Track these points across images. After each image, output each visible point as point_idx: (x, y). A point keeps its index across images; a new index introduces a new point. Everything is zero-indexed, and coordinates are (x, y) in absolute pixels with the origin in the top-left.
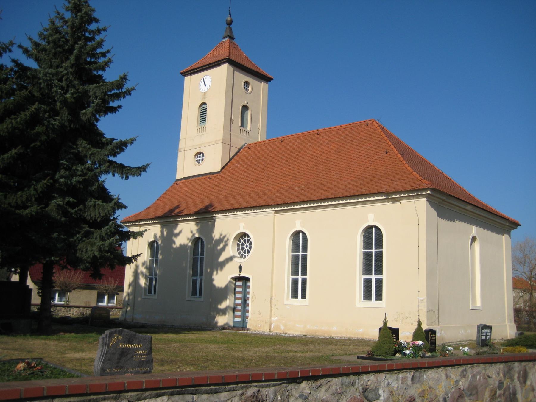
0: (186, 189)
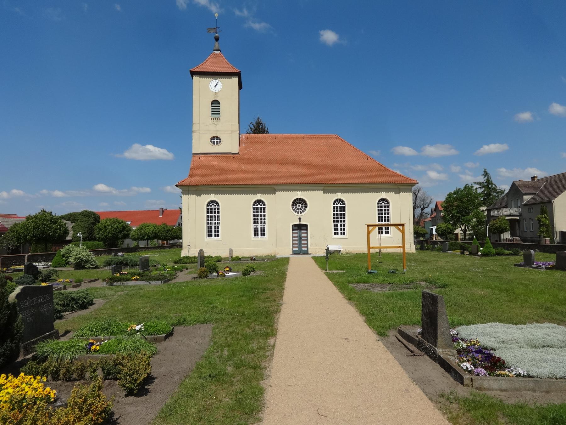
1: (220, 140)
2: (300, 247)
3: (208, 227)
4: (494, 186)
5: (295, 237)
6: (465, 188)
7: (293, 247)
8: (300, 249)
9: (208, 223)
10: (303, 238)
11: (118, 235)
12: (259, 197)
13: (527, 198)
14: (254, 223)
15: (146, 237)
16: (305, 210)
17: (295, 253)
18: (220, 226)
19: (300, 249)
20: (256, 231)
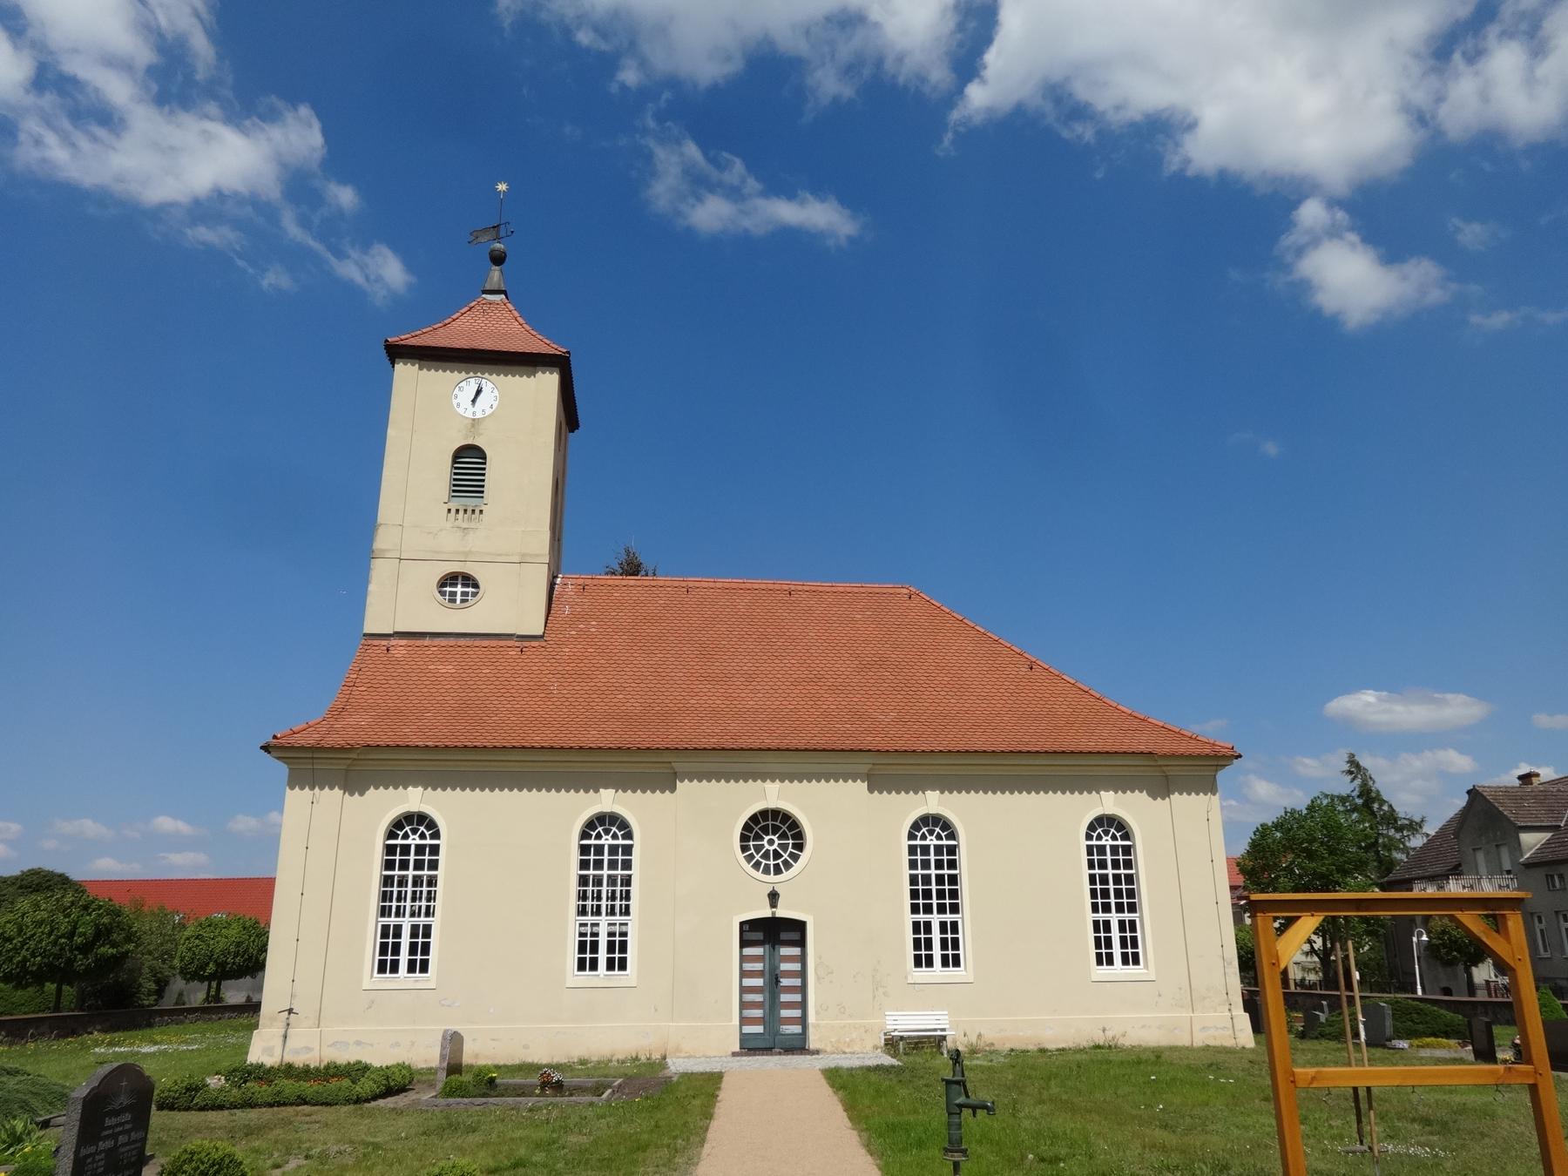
1: (476, 586)
2: (771, 1020)
3: (385, 929)
4: (1385, 808)
5: (751, 974)
6: (1311, 808)
7: (744, 1021)
8: (774, 1032)
9: (384, 912)
10: (785, 982)
11: (70, 962)
12: (607, 800)
13: (1532, 841)
14: (582, 911)
15: (211, 968)
16: (795, 858)
17: (750, 1047)
18: (436, 922)
19: (774, 1032)
20: (587, 946)
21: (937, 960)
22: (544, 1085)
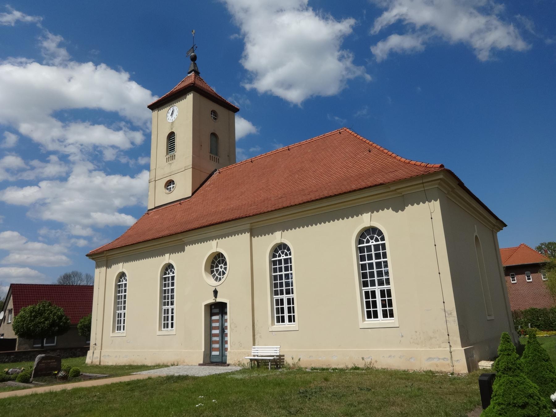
0: (157, 217)
3: (367, 293)
12: (366, 220)
18: (392, 287)
21: (380, 314)
22: (410, 397)
